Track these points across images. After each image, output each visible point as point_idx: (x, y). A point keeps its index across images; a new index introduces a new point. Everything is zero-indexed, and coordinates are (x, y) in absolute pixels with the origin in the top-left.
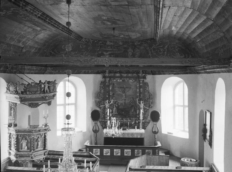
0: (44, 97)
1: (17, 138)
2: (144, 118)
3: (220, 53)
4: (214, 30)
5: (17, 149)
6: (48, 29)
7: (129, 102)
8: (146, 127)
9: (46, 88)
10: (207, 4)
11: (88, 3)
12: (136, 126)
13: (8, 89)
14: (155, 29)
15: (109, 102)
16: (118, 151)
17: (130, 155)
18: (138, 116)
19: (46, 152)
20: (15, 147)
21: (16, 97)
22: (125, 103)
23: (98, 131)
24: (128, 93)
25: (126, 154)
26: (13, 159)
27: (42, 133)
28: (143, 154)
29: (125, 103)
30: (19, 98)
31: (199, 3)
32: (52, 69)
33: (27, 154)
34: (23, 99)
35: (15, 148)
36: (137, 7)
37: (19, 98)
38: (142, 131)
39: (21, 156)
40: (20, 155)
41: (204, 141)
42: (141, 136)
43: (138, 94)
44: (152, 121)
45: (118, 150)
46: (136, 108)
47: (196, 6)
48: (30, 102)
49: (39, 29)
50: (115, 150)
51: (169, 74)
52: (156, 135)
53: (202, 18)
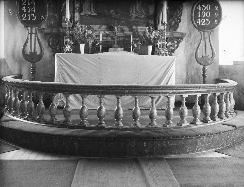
12: (149, 44)
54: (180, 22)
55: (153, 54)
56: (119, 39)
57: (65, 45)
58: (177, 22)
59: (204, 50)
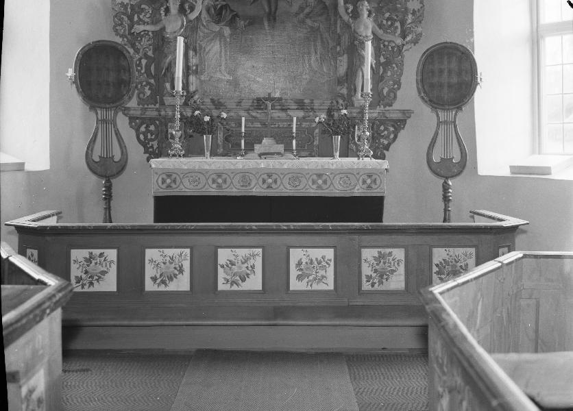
12: (337, 134)
16: (245, 261)
23: (122, 167)
25: (299, 278)
54: (399, 88)
55: (539, 154)
56: (277, 126)
57: (171, 140)
58: (393, 89)
59: (107, 146)
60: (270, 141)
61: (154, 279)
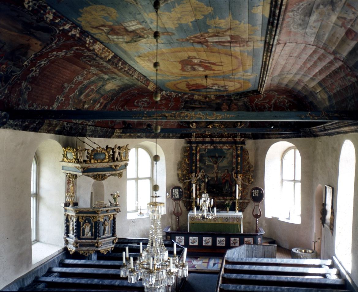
0: (113, 167)
1: (78, 222)
2: (242, 197)
3: (350, 105)
4: (343, 74)
5: (78, 236)
6: (118, 78)
7: (223, 177)
8: (245, 209)
9: (117, 155)
10: (337, 38)
11: (177, 40)
13: (65, 156)
14: (260, 75)
15: (195, 176)
16: (208, 240)
17: (224, 245)
18: (234, 195)
19: (115, 239)
20: (75, 233)
21: (76, 167)
22: (217, 177)
24: (221, 165)
25: (219, 243)
26: (72, 248)
27: (110, 214)
28: (241, 243)
29: (217, 177)
30: (81, 168)
31: (326, 37)
32: (121, 131)
33: (91, 243)
34: (86, 169)
35: (75, 234)
36: (242, 45)
37: (81, 168)
38: (238, 214)
39: (83, 245)
40: (81, 243)
41: (323, 226)
42: (238, 221)
43: (235, 166)
44: (252, 202)
45: (208, 238)
46: (231, 183)
47: (321, 42)
48: (95, 173)
49: (106, 77)
50: (204, 238)
51: (277, 138)
52: (257, 220)
53: (327, 59)
60: (225, 160)
61: (191, 243)
